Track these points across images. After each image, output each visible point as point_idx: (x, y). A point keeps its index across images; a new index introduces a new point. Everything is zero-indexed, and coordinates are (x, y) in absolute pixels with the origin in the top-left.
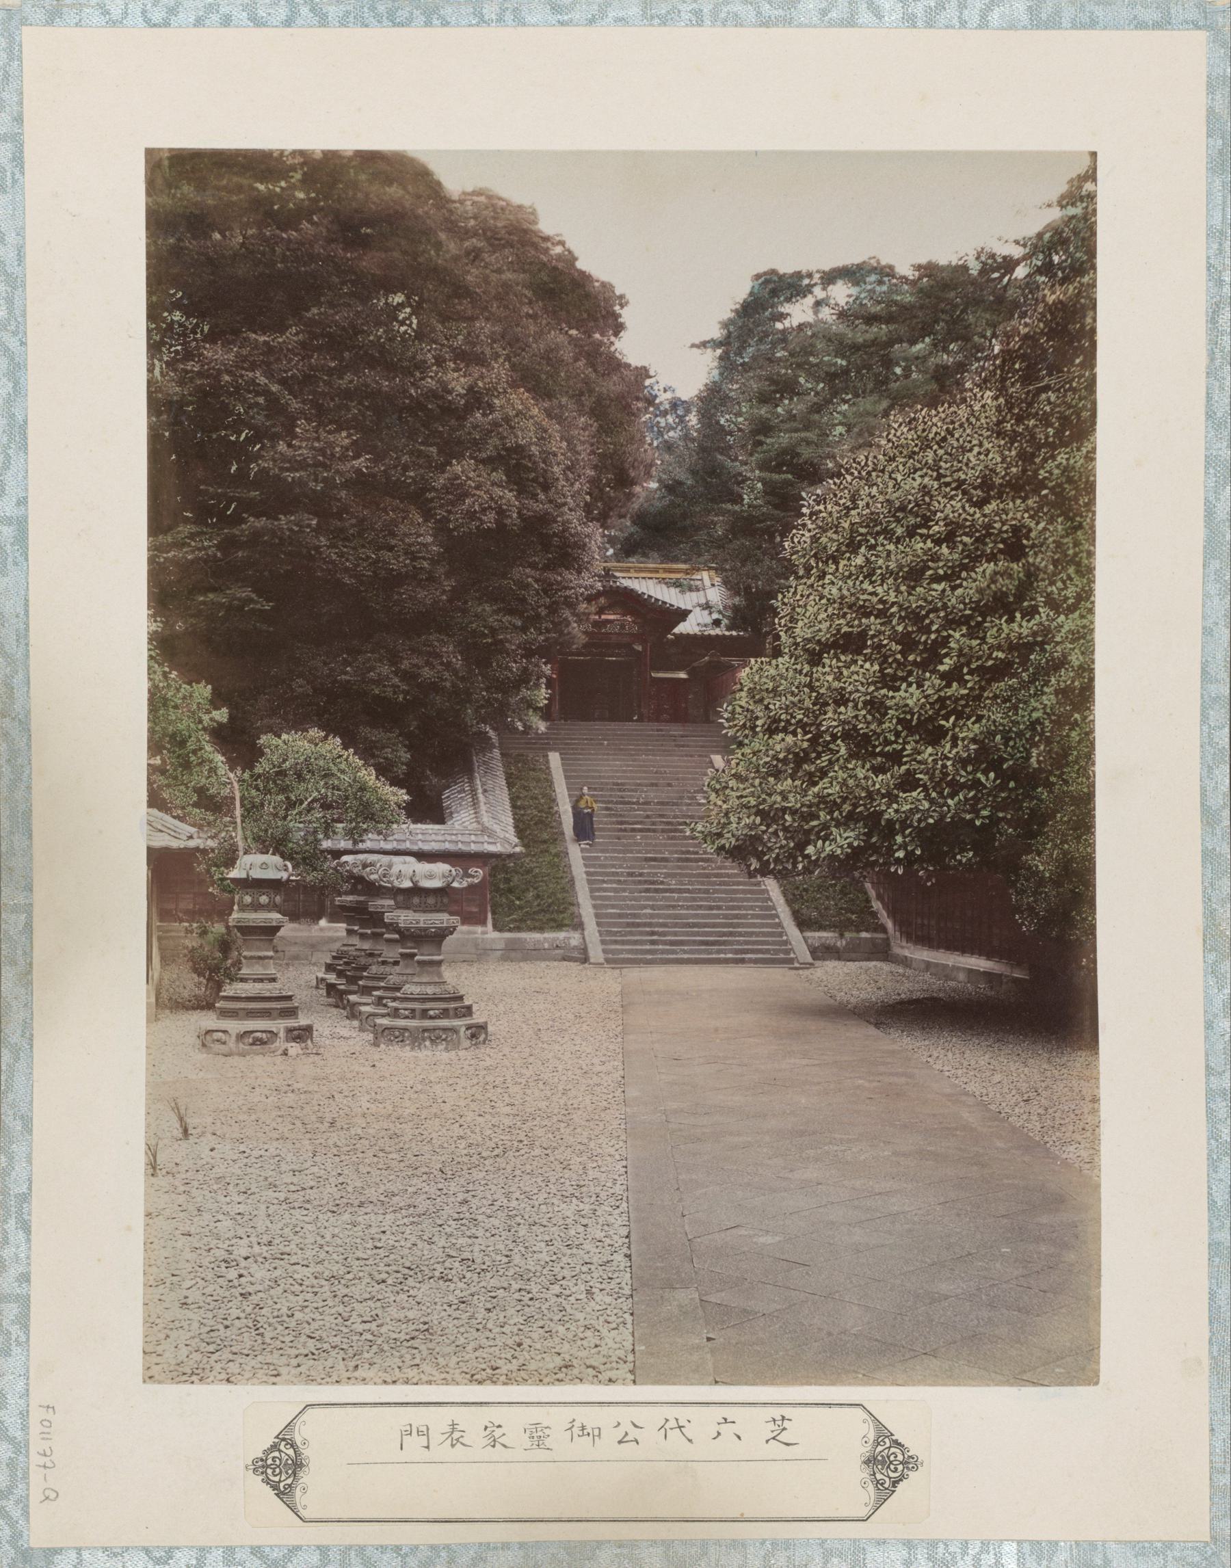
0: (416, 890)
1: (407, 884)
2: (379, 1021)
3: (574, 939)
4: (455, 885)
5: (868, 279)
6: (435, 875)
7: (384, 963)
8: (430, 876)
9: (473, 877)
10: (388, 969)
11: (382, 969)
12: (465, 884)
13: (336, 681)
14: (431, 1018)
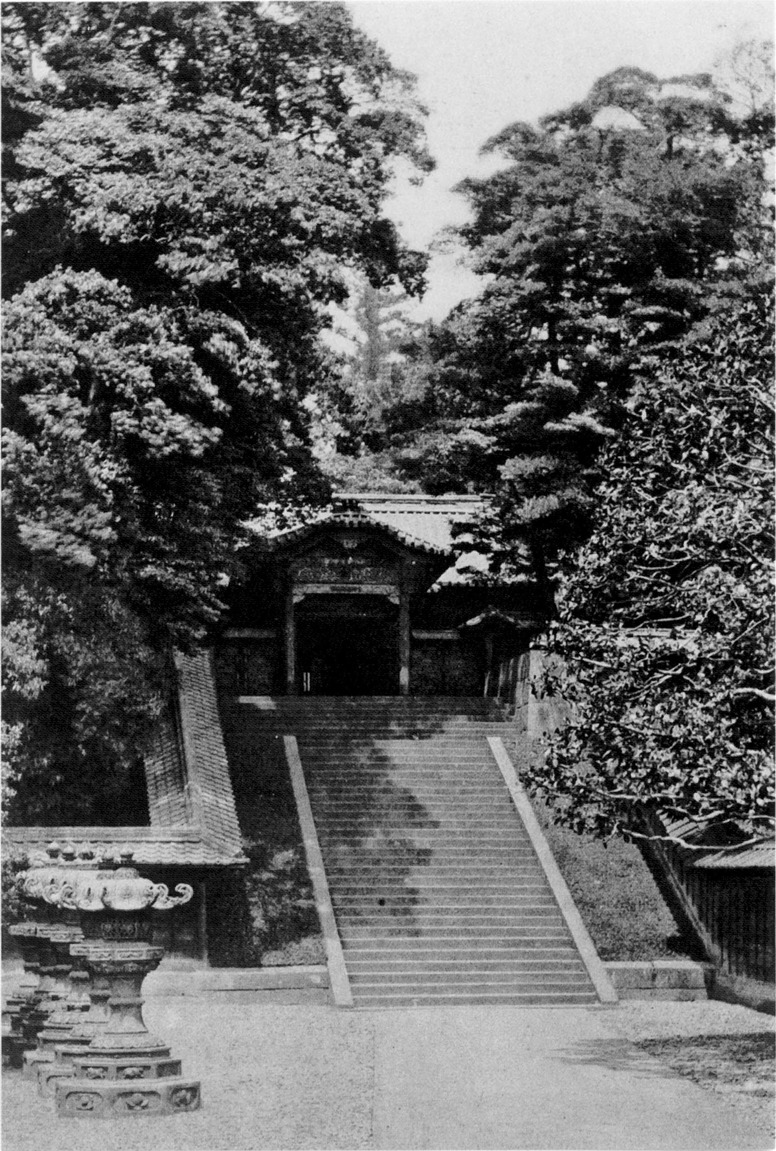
0: (108, 914)
1: (96, 905)
2: (65, 1083)
3: (314, 972)
4: (158, 905)
5: (302, 598)
6: (130, 893)
7: (70, 1008)
8: (127, 895)
9: (181, 895)
10: (75, 1015)
11: (68, 1017)
12: (170, 905)
13: (241, 880)
14: (128, 1077)
